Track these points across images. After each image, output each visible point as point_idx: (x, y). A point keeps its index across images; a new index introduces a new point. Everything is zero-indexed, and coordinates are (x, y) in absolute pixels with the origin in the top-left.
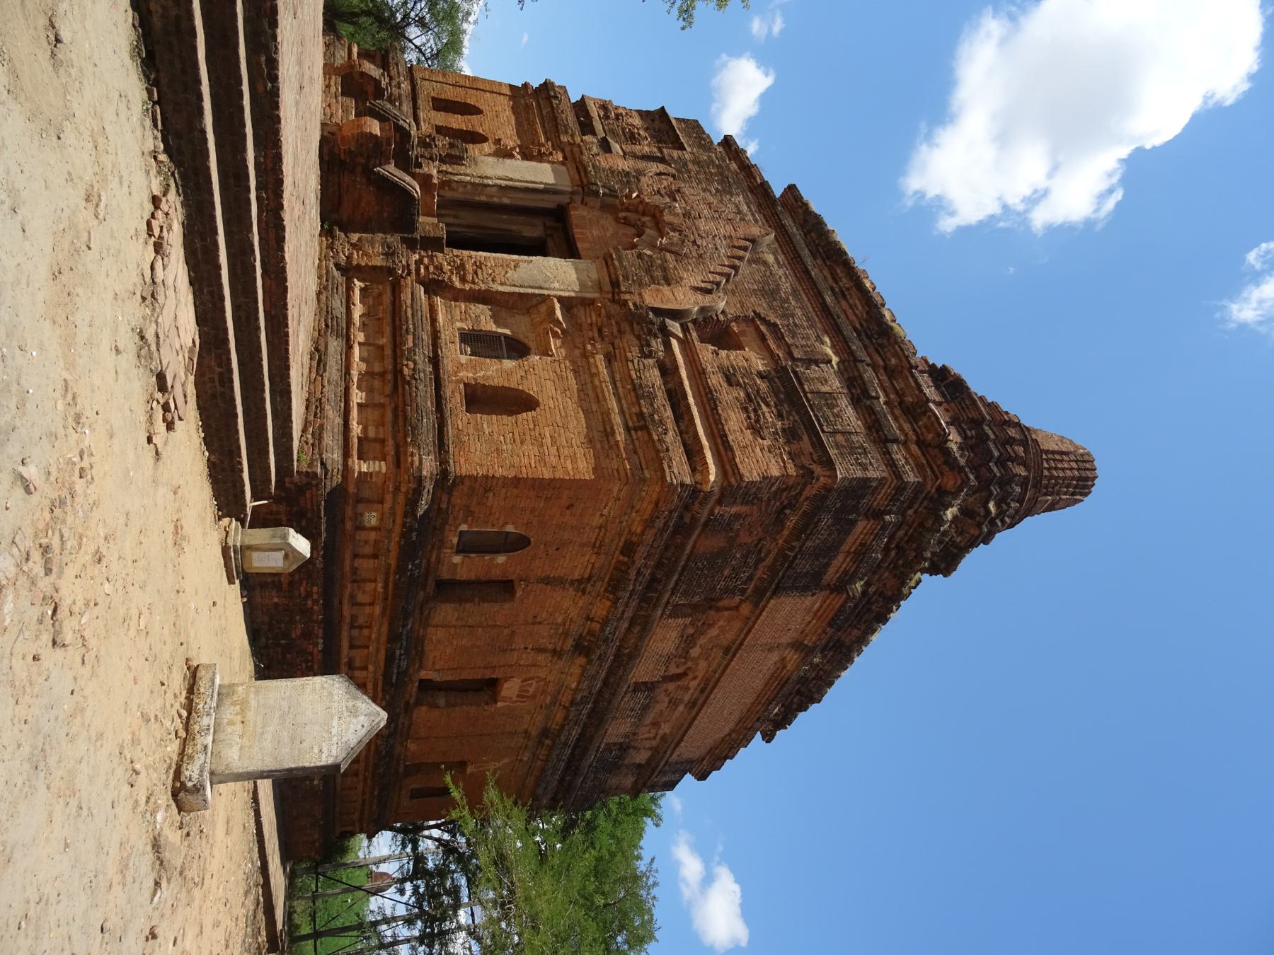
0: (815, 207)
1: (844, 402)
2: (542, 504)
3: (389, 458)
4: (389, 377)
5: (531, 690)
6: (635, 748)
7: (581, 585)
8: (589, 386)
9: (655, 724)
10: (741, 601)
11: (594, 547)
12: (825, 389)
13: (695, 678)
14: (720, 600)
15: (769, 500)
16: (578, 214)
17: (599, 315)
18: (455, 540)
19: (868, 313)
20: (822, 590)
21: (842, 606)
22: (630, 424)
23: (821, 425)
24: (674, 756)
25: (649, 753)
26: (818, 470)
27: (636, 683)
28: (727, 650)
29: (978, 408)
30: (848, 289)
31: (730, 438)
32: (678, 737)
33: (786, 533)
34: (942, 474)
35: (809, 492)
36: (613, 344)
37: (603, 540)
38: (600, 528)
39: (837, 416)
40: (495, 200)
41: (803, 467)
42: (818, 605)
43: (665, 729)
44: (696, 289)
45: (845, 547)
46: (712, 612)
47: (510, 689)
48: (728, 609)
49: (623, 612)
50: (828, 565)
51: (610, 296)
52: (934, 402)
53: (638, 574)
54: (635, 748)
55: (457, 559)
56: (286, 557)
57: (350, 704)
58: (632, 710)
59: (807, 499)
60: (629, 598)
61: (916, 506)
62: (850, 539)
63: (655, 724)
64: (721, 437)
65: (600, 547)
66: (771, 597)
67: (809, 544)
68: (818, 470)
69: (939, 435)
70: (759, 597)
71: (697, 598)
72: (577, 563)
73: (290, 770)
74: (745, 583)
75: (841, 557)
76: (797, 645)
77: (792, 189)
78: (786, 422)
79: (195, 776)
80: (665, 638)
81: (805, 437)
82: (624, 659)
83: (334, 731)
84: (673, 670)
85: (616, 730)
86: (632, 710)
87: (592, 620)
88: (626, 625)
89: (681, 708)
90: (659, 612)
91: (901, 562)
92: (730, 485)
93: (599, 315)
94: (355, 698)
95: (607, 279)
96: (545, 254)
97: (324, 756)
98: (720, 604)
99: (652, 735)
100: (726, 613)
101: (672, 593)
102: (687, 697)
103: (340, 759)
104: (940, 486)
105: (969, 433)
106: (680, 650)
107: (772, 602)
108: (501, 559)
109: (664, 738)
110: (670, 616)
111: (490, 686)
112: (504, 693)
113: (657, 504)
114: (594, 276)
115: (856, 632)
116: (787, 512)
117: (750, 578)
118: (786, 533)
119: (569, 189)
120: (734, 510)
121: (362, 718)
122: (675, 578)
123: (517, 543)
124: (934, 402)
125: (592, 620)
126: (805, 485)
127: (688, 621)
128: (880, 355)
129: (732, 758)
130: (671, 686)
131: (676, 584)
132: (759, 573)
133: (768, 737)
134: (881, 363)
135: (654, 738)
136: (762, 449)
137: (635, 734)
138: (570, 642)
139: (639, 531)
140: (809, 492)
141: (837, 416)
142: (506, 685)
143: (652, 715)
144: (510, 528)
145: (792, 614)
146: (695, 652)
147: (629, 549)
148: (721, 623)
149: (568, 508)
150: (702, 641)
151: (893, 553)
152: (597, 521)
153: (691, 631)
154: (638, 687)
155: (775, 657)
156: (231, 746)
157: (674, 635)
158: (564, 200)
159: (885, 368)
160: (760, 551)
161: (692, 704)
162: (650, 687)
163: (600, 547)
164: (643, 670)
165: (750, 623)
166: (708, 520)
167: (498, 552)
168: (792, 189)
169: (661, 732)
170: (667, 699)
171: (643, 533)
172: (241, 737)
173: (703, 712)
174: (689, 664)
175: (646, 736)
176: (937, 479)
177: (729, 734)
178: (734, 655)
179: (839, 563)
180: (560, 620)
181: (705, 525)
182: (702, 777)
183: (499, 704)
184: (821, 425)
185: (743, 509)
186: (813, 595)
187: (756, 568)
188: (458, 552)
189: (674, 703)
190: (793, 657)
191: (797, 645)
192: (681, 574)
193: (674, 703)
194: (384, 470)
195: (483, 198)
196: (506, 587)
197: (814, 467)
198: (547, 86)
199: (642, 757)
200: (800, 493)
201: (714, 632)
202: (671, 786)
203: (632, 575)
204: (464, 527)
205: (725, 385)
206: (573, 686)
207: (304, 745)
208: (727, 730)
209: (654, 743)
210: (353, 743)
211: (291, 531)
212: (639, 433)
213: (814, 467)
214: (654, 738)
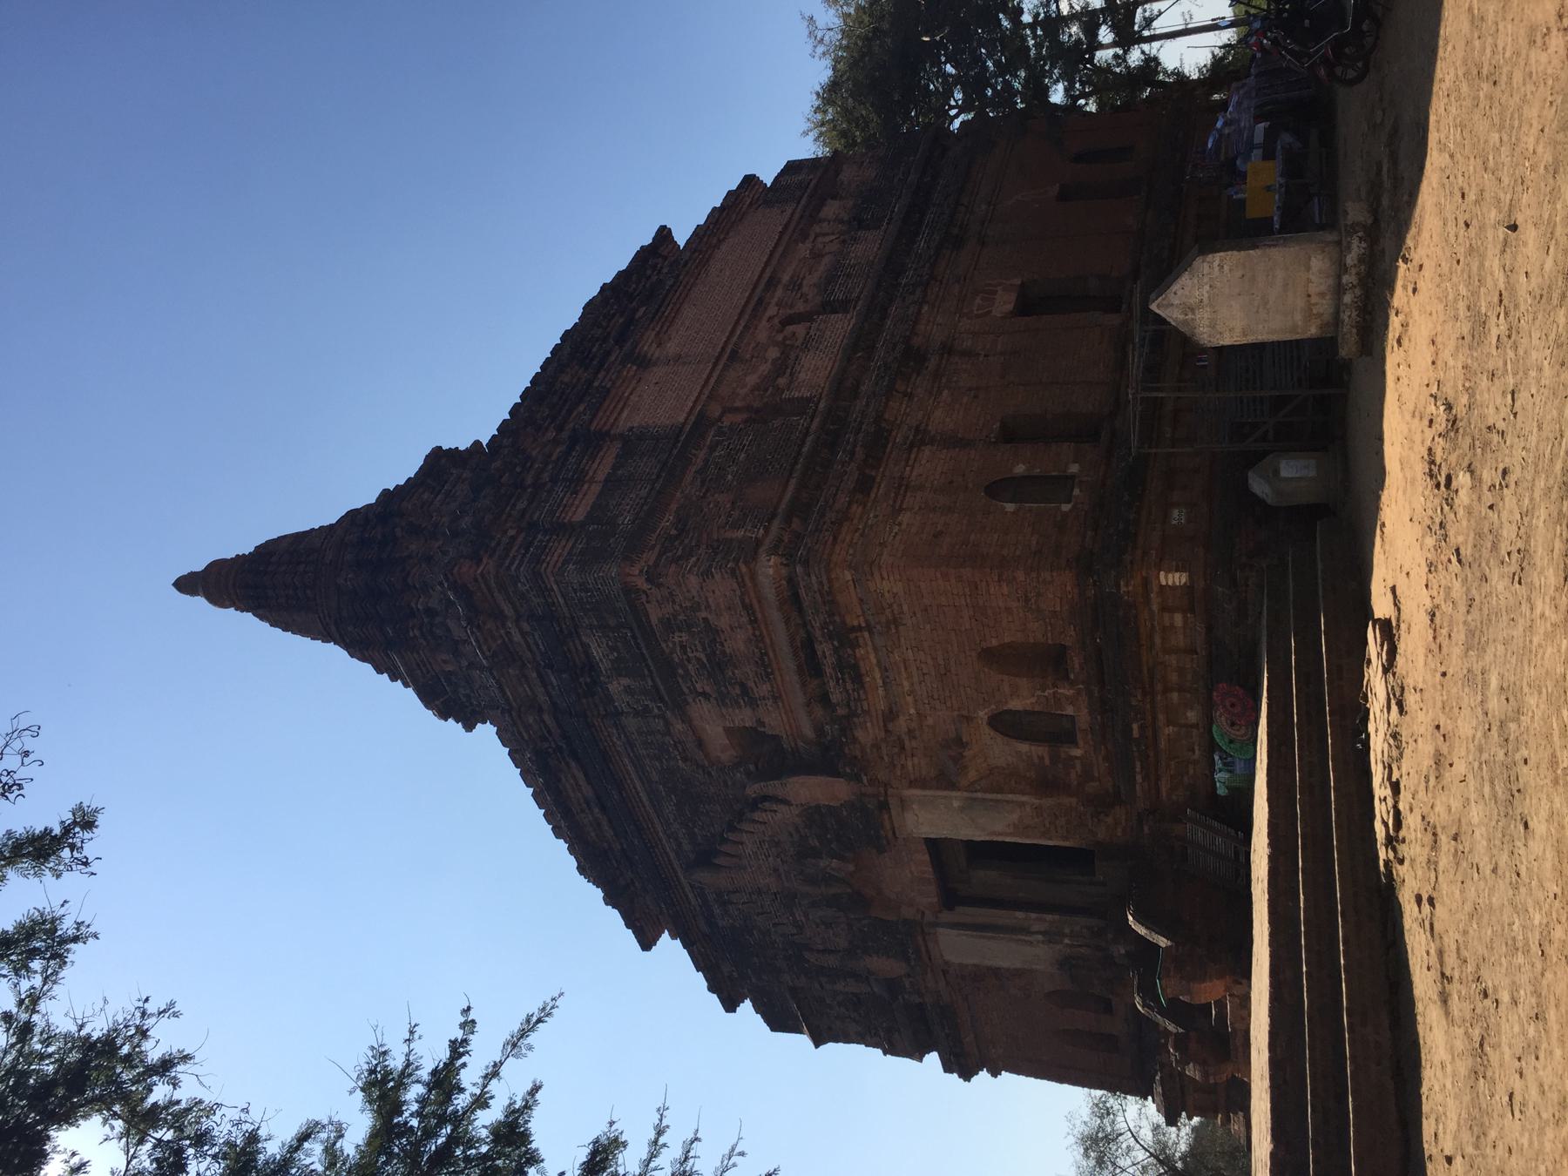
0: (614, 916)
1: (604, 666)
2: (972, 537)
3: (1156, 589)
4: (1159, 687)
5: (978, 301)
6: (842, 222)
7: (922, 437)
8: (916, 679)
9: (817, 256)
10: (720, 419)
11: (907, 487)
12: (625, 681)
13: (770, 319)
14: (746, 421)
15: (698, 546)
16: (927, 897)
17: (903, 766)
18: (1076, 492)
19: (559, 780)
20: (621, 435)
21: (594, 416)
22: (866, 634)
23: (634, 637)
24: (789, 211)
25: (822, 215)
26: (642, 583)
27: (846, 311)
28: (734, 356)
29: (405, 665)
30: (583, 811)
31: (745, 619)
32: (786, 238)
33: (674, 507)
34: (476, 580)
35: (651, 557)
36: (887, 731)
37: (897, 495)
38: (901, 510)
39: (612, 649)
40: (1033, 915)
41: (659, 586)
42: (624, 415)
43: (804, 249)
44: (787, 803)
45: (596, 488)
46: (756, 404)
47: (1004, 303)
48: (737, 410)
49: (867, 405)
50: (615, 468)
51: (890, 791)
52: (482, 668)
53: (853, 453)
54: (842, 222)
55: (1074, 469)
56: (1276, 472)
57: (1190, 316)
58: (849, 276)
59: (653, 547)
60: (861, 423)
61: (505, 540)
62: (590, 499)
63: (817, 256)
64: (756, 620)
65: (900, 486)
66: (684, 424)
67: (644, 493)
68: (642, 583)
69: (479, 627)
70: (701, 423)
71: (777, 423)
72: (929, 465)
73: (1254, 247)
74: (718, 443)
75: (601, 476)
76: (644, 363)
77: (647, 943)
78: (677, 639)
79: (1355, 242)
80: (815, 371)
81: (654, 620)
82: (860, 344)
83: (1207, 287)
84: (800, 330)
85: (869, 247)
86: (849, 276)
87: (905, 394)
88: (863, 388)
89: (786, 278)
90: (822, 405)
91: (518, 469)
92: (745, 563)
93: (903, 766)
94: (1185, 322)
95: (893, 813)
96: (970, 844)
97: (1216, 264)
98: (745, 416)
99: (820, 239)
100: (738, 404)
101: (808, 429)
102: (779, 292)
103: (1199, 260)
104: (478, 565)
105: (417, 632)
106: (793, 356)
107: (681, 419)
108: (1020, 469)
109: (804, 236)
110: (809, 400)
111: (1026, 306)
112: (1013, 296)
113: (835, 539)
114: (909, 816)
115: (566, 379)
116: (674, 532)
117: (712, 449)
118: (674, 507)
119: (940, 930)
120: (740, 533)
121: (1177, 302)
122: (805, 449)
123: (998, 489)
124: (482, 668)
125: (905, 394)
126: (656, 564)
127: (786, 395)
128: (546, 726)
129: (714, 209)
130: (800, 307)
131: (803, 442)
132: (702, 454)
133: (664, 234)
134: (546, 717)
135: (817, 236)
136: (708, 607)
137: (844, 241)
138: (932, 363)
139: (854, 507)
140: (651, 557)
141: (612, 649)
142: (1010, 307)
143: (822, 268)
144: (1010, 507)
145: (657, 401)
146: (773, 353)
147: (864, 486)
148: (743, 392)
149: (941, 533)
150: (765, 368)
151: (529, 481)
152: (905, 518)
153: (782, 381)
154: (843, 306)
155: (672, 347)
156: (1320, 272)
157: (802, 376)
158: (946, 916)
159: (540, 710)
160: (703, 482)
161: (772, 283)
162: (829, 307)
163: (900, 486)
164: (839, 327)
165: (707, 392)
166: (770, 521)
167: (1024, 478)
168: (647, 943)
169: (808, 244)
170: (805, 289)
171: (850, 504)
172: (1309, 281)
173: (757, 274)
174: (780, 338)
175: (827, 239)
176: (482, 575)
177: (720, 241)
178: (723, 349)
179: (602, 467)
180: (945, 393)
181: (773, 516)
182: (750, 181)
183: (1018, 282)
184: (634, 637)
185: (729, 535)
186: (631, 429)
187: (706, 461)
188: (1073, 477)
189: (795, 285)
190: (648, 346)
191: (644, 363)
192: (799, 453)
193: (795, 285)
194: (1162, 574)
195: (1049, 917)
196: (1010, 435)
197: (646, 586)
198: (967, 1075)
199: (831, 209)
200: (660, 556)
201: (752, 380)
202: (792, 168)
203: (860, 453)
204: (1066, 507)
205: (751, 684)
206: (926, 308)
207: (1239, 274)
208: (724, 247)
209: (817, 229)
210: (1186, 276)
211: (1269, 501)
212: (856, 623)
213: (646, 586)
214: (817, 236)
